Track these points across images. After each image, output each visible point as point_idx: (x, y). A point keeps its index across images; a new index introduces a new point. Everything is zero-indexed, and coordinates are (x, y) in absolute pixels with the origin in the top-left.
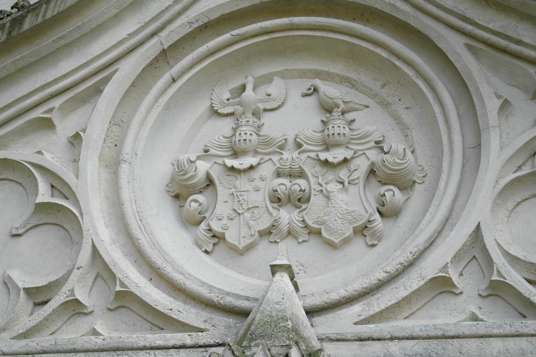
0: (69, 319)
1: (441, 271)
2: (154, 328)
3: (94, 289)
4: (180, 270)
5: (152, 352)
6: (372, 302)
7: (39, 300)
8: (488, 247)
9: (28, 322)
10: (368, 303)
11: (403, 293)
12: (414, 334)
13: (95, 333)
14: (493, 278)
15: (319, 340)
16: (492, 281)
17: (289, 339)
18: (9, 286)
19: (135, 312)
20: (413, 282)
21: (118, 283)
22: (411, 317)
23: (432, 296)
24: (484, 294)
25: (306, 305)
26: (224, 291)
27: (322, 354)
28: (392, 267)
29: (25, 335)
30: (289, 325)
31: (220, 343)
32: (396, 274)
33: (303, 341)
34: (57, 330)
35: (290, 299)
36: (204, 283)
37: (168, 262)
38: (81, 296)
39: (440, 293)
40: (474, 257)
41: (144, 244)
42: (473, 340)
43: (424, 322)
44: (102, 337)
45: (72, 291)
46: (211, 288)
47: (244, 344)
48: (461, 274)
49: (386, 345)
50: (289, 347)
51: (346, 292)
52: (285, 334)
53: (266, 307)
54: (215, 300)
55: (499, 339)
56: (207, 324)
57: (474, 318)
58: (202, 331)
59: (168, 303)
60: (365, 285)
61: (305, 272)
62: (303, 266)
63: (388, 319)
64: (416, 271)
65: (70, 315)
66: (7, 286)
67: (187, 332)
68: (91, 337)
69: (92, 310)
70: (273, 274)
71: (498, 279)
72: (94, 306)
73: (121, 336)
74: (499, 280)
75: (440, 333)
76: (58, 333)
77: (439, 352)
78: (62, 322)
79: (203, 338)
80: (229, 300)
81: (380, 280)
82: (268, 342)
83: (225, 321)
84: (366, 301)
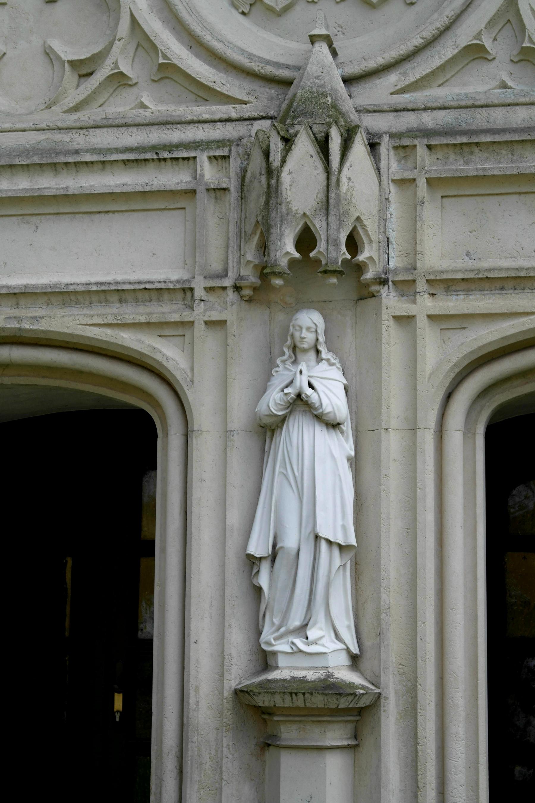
0: (115, 91)
1: (475, 38)
2: (198, 99)
3: (136, 60)
4: (219, 37)
5: (200, 126)
6: (407, 72)
7: (84, 72)
8: (521, 12)
9: (77, 96)
10: (404, 73)
11: (437, 62)
12: (446, 104)
13: (143, 106)
14: (524, 45)
15: (356, 111)
16: (523, 48)
17: (329, 116)
18: (52, 57)
19: (179, 83)
20: (447, 50)
21: (160, 55)
22: (445, 85)
23: (466, 62)
24: (516, 60)
25: (344, 74)
26: (264, 59)
27: (359, 130)
28: (428, 33)
29: (76, 109)
30: (328, 101)
31: (264, 115)
32: (432, 39)
33: (342, 117)
34: (105, 102)
35: (329, 73)
36: (244, 51)
37: (207, 29)
38: (124, 68)
39: (474, 59)
40: (509, 20)
41: (181, 11)
42: (500, 109)
43: (457, 90)
44: (150, 110)
45: (116, 64)
46: (251, 57)
47: (288, 122)
48: (495, 39)
49: (419, 115)
50: (329, 125)
51: (383, 60)
52: (325, 111)
53: (307, 83)
54: (256, 70)
55: (524, 108)
56: (250, 96)
57: (504, 86)
58: (245, 103)
59: (211, 76)
60: (402, 52)
61: (344, 33)
62: (342, 27)
63: (424, 87)
64: (452, 38)
65: (116, 86)
66: (50, 57)
67: (231, 104)
68: (140, 110)
69: (136, 81)
70: (313, 43)
71: (529, 45)
72: (138, 77)
73: (169, 109)
74: (530, 47)
75: (470, 103)
76: (106, 105)
77: (469, 121)
78: (109, 94)
79: (247, 111)
80: (269, 70)
81: (416, 47)
82: (310, 120)
83: (268, 93)
84: (402, 70)
